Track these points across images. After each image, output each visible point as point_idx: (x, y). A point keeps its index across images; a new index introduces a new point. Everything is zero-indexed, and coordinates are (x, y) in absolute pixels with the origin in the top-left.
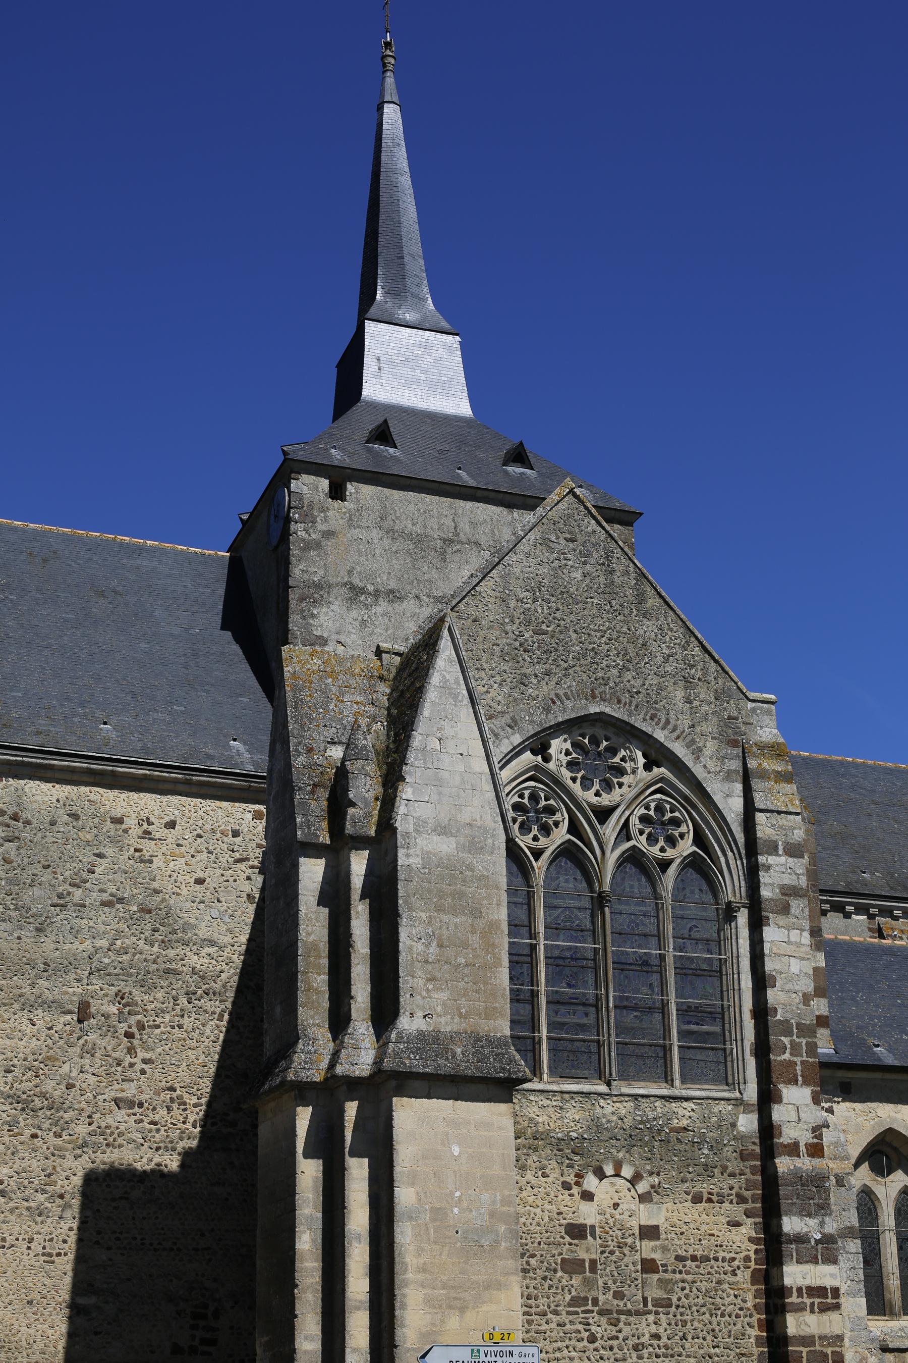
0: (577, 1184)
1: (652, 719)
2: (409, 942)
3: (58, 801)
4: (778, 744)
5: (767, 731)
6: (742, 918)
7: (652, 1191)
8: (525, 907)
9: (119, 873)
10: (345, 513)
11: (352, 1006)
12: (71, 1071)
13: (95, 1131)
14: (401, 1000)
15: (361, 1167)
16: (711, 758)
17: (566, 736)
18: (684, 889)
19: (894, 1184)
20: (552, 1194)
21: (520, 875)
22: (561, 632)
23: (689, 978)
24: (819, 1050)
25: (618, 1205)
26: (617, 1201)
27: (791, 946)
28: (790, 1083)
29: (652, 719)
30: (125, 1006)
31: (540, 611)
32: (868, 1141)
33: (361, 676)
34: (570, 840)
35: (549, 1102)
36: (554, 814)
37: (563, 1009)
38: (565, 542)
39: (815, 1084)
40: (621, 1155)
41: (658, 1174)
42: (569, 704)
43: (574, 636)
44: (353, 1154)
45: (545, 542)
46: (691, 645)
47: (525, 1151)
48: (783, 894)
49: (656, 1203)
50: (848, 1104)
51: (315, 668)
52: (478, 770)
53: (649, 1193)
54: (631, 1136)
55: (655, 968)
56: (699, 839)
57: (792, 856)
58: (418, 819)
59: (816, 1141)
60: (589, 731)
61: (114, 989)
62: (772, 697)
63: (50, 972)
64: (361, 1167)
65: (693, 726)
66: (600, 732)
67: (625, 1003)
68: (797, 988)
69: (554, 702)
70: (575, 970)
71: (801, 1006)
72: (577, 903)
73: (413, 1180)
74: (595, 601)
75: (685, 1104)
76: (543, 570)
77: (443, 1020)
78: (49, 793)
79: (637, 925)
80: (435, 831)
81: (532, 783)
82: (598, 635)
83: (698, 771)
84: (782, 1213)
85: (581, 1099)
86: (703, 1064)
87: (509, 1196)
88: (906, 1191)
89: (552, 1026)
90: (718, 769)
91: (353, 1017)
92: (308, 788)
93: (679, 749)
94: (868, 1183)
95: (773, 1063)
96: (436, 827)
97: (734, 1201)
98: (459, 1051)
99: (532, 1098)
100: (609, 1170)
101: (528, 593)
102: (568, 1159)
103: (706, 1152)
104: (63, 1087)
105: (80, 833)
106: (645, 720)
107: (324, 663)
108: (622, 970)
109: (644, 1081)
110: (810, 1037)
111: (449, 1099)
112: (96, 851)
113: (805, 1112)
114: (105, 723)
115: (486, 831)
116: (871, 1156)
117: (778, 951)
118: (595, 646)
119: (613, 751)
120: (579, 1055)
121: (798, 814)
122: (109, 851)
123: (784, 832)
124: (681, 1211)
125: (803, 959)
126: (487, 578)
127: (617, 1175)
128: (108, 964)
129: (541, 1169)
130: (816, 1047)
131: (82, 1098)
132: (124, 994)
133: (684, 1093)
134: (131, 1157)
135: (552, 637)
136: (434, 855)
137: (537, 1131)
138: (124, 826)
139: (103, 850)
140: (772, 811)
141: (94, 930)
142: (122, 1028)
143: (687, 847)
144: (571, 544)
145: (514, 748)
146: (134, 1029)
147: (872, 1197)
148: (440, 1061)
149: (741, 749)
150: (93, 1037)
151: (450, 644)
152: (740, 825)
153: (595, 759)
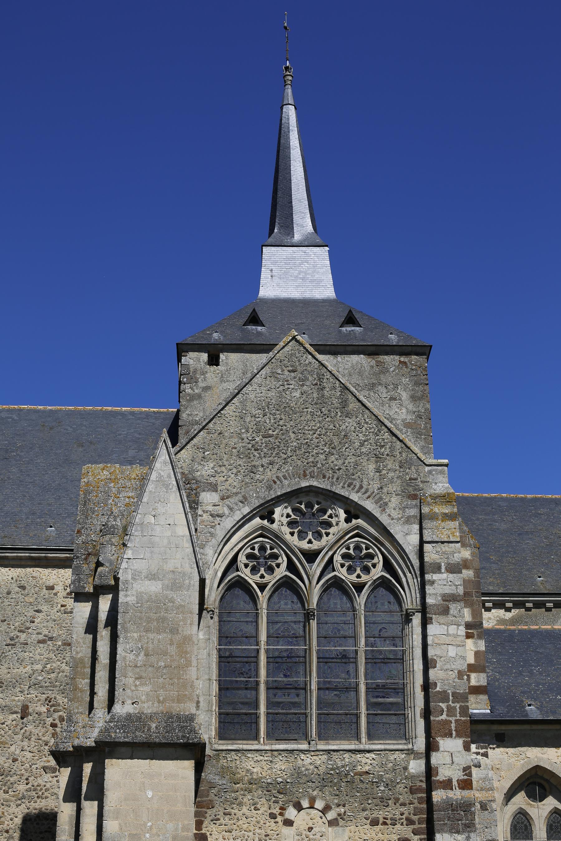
0: (281, 814)
1: (349, 486)
2: (124, 654)
3: (12, 578)
4: (449, 494)
5: (441, 485)
6: (417, 620)
7: (339, 818)
8: (254, 624)
9: (51, 621)
10: (218, 373)
11: (95, 699)
12: (15, 750)
13: (30, 788)
14: (116, 693)
15: (92, 807)
16: (394, 509)
17: (286, 505)
18: (376, 602)
19: (544, 807)
20: (262, 822)
21: (251, 603)
22: (283, 434)
23: (378, 665)
24: (471, 711)
25: (312, 828)
26: (311, 825)
27: (449, 637)
28: (446, 737)
29: (349, 486)
30: (51, 706)
31: (268, 422)
32: (518, 775)
33: (135, 479)
34: (286, 575)
35: (262, 758)
36: (277, 559)
37: (279, 692)
38: (288, 373)
39: (466, 736)
40: (315, 793)
41: (344, 806)
42: (286, 482)
43: (293, 436)
44: (86, 799)
45: (273, 375)
46: (382, 432)
47: (242, 792)
48: (444, 600)
49: (341, 827)
50: (502, 749)
51: (103, 478)
52: (181, 533)
53: (336, 819)
54: (323, 779)
55: (352, 660)
56: (388, 566)
57: (451, 573)
58: (135, 570)
59: (466, 777)
60: (305, 499)
61: (45, 696)
62: (446, 461)
63: (4, 687)
64: (92, 807)
65: (381, 488)
66: (313, 500)
67: (328, 686)
68: (453, 667)
69: (275, 482)
70: (290, 665)
71: (456, 680)
72: (293, 619)
73: (117, 815)
74: (309, 410)
75: (368, 755)
76: (270, 394)
77: (146, 705)
78: (6, 574)
79: (339, 630)
80: (147, 578)
81: (261, 539)
82: (311, 433)
83: (384, 519)
84: (436, 831)
85: (286, 755)
86: (388, 726)
87: (188, 824)
88: (556, 811)
89: (269, 704)
90: (400, 516)
91: (95, 707)
92: (83, 557)
93: (369, 505)
94: (523, 807)
95: (432, 722)
96: (148, 575)
97: (405, 823)
98: (154, 726)
99: (249, 755)
100: (305, 804)
101: (260, 411)
102: (274, 797)
103: (382, 788)
104: (10, 761)
105: (26, 598)
106: (343, 487)
107: (110, 474)
108: (326, 663)
109: (340, 739)
110: (462, 702)
111: (146, 759)
112: (36, 609)
113: (457, 757)
114: (51, 527)
115: (184, 574)
116: (528, 785)
117: (439, 642)
118: (308, 441)
119: (324, 511)
120: (291, 724)
121: (458, 542)
122: (44, 608)
123: (446, 556)
124: (361, 831)
125: (459, 646)
126: (230, 404)
127: (312, 807)
128: (41, 680)
129: (253, 805)
130: (468, 709)
131: (23, 767)
132: (51, 699)
133: (367, 747)
134: (53, 804)
135: (276, 438)
136: (145, 594)
137: (252, 778)
138: (54, 591)
139: (40, 607)
140: (437, 542)
141: (33, 659)
142: (49, 721)
143: (378, 572)
144: (293, 374)
145: (244, 516)
146: (57, 721)
147: (528, 817)
148: (137, 733)
149: (419, 500)
150: (30, 727)
151: (165, 451)
152: (416, 554)
153: (310, 518)
